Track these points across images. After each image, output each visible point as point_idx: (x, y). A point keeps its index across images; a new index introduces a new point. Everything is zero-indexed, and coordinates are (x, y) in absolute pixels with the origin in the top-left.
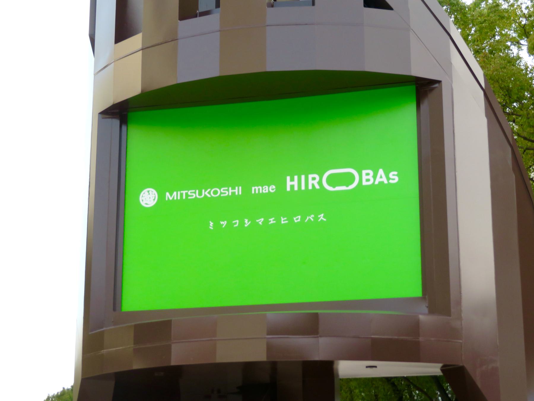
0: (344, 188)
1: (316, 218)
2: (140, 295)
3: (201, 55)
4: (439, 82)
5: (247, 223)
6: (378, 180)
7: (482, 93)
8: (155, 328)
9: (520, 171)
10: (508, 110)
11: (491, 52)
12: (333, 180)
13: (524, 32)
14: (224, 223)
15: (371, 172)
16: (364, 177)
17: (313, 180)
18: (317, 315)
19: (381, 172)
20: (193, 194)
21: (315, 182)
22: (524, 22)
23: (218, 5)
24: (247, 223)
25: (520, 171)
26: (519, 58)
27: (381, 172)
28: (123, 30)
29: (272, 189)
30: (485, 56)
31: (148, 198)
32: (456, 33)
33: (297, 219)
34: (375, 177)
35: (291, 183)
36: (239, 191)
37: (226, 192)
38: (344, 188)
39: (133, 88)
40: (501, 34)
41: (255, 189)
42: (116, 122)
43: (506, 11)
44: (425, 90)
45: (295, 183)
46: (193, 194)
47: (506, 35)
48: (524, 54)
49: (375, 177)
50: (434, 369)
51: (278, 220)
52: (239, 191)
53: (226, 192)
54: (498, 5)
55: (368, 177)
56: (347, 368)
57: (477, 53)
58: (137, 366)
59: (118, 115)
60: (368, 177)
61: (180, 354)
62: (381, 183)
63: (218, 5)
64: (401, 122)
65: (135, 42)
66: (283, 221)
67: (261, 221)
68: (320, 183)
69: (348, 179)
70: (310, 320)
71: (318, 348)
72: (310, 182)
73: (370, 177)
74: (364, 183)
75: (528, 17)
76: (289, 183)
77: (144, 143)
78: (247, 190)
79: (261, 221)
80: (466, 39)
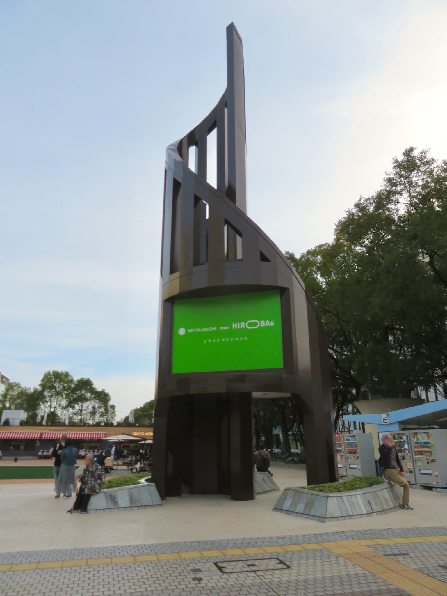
0: (254, 327)
1: (244, 339)
2: (179, 367)
3: (201, 279)
4: (288, 288)
5: (218, 340)
6: (267, 324)
7: (304, 292)
8: (185, 380)
9: (319, 319)
10: (313, 297)
11: (307, 276)
12: (250, 325)
13: (319, 269)
14: (210, 341)
15: (264, 322)
16: (261, 324)
17: (242, 325)
18: (244, 375)
19: (268, 321)
20: (198, 330)
21: (243, 325)
22: (319, 265)
23: (207, 261)
24: (223, 340)
25: (319, 319)
26: (317, 278)
27: (268, 321)
28: (173, 270)
29: (227, 328)
30: (305, 278)
31: (182, 331)
32: (294, 269)
33: (237, 339)
34: (265, 323)
35: (234, 326)
36: (215, 329)
37: (210, 329)
38: (254, 327)
39: (176, 291)
40: (310, 270)
41: (221, 328)
42: (170, 304)
43: (312, 261)
44: (283, 292)
45: (236, 326)
46: (198, 330)
47: (312, 270)
48: (319, 277)
49: (265, 323)
50: (288, 395)
51: (234, 340)
52: (215, 329)
53: (210, 329)
54: (309, 259)
55: (262, 324)
56: (256, 395)
57: (302, 277)
58: (178, 394)
59: (170, 303)
60: (262, 324)
61: (194, 390)
62: (268, 326)
63: (207, 261)
64: (274, 304)
65: (177, 274)
66: (232, 340)
67: (210, 341)
68: (245, 326)
69: (255, 324)
70: (241, 377)
71: (244, 387)
72: (242, 325)
73: (264, 323)
74: (262, 326)
75: (320, 263)
76: (234, 326)
77: (180, 312)
78: (218, 328)
79: (223, 340)
80: (297, 272)
